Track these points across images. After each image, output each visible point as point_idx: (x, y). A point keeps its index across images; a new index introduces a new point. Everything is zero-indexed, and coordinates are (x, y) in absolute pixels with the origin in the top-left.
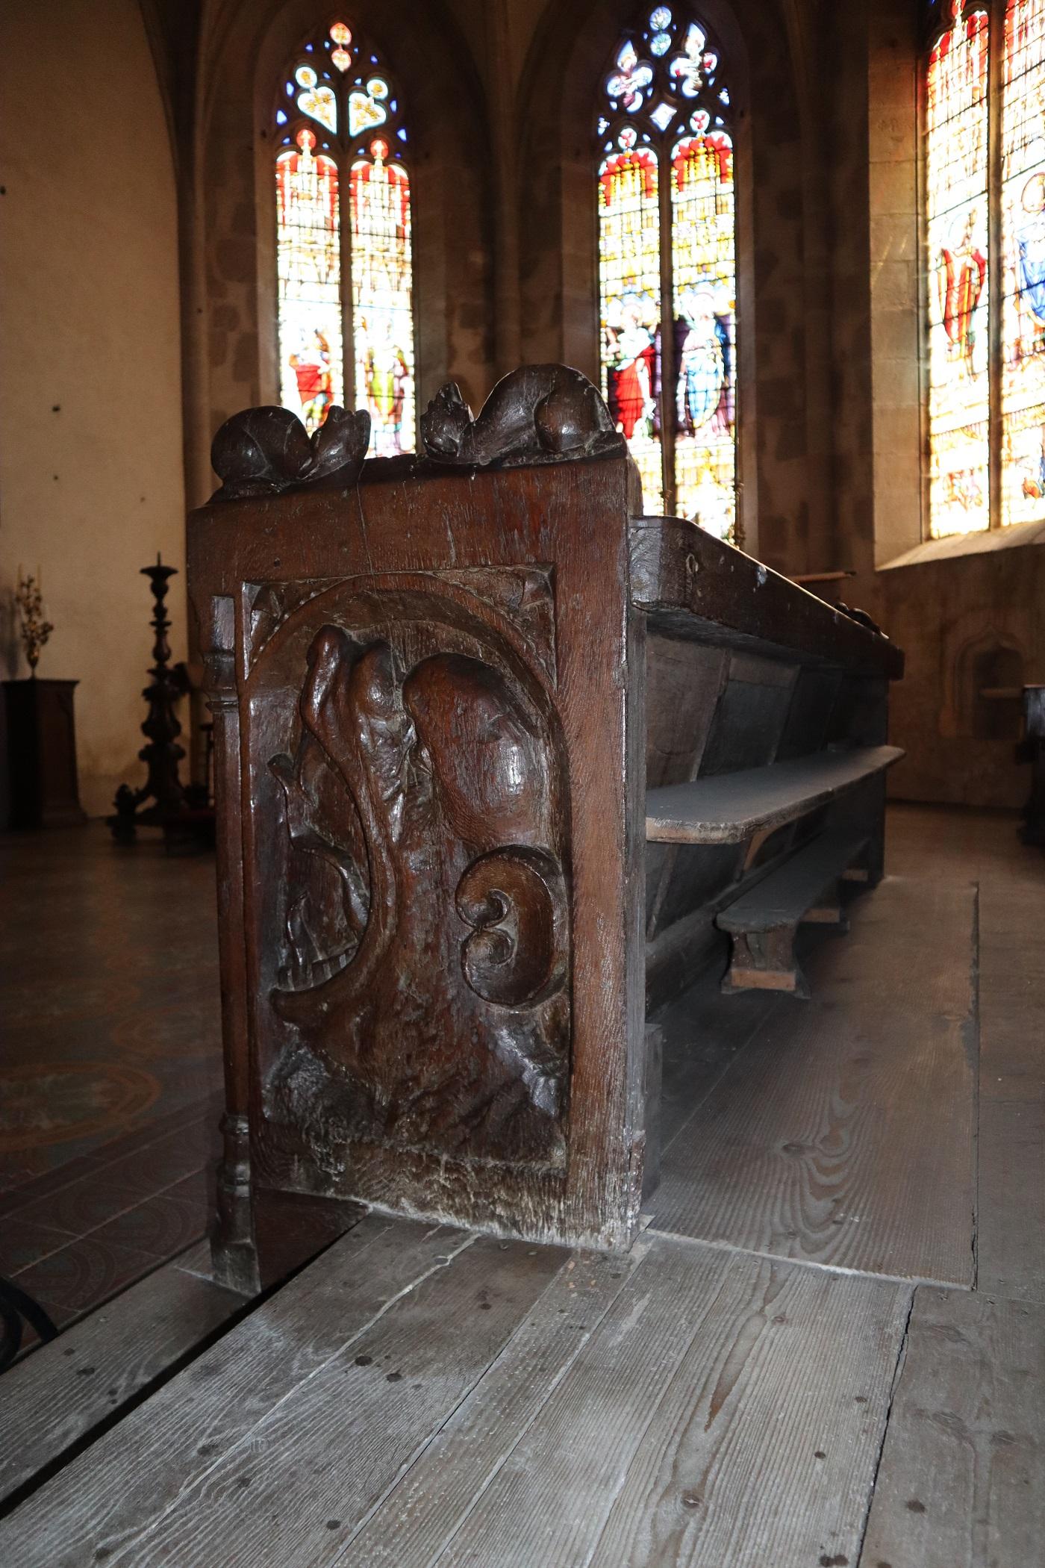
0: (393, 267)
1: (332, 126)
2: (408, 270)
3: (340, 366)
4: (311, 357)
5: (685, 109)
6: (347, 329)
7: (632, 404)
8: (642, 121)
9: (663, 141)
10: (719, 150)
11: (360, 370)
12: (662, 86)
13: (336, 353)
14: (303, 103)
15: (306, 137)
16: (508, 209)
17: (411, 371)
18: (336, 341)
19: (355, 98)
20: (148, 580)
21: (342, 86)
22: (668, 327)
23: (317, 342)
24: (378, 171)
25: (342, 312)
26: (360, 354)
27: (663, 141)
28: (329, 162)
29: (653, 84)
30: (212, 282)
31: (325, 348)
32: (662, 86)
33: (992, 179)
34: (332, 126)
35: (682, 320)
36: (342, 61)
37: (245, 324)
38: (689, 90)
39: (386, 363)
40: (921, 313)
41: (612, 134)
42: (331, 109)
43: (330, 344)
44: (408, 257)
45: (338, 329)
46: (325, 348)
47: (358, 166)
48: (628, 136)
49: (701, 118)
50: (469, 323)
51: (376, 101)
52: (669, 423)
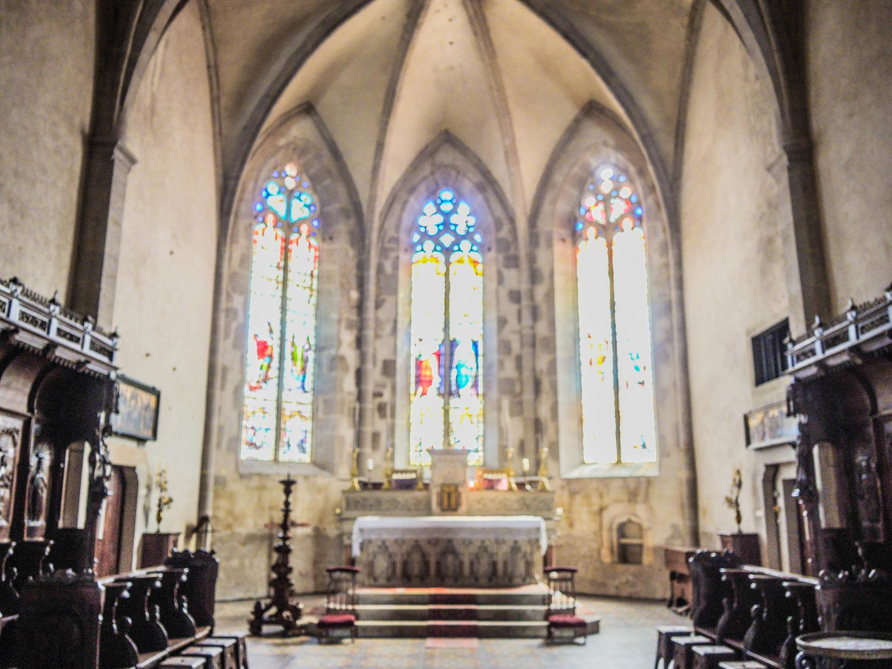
0: (308, 291)
1: (282, 213)
2: (315, 294)
3: (279, 342)
4: (264, 337)
5: (459, 239)
6: (283, 322)
7: (428, 379)
8: (436, 239)
9: (448, 251)
10: (475, 263)
11: (288, 345)
12: (446, 226)
13: (277, 334)
14: (270, 202)
15: (270, 218)
16: (372, 273)
17: (313, 348)
18: (277, 328)
19: (295, 202)
20: (282, 487)
21: (290, 194)
22: (448, 343)
23: (268, 328)
24: (303, 240)
25: (282, 313)
26: (288, 337)
27: (448, 251)
28: (281, 233)
29: (443, 224)
30: (228, 295)
31: (271, 331)
32: (446, 226)
33: (210, 45)
34: (282, 213)
35: (454, 340)
36: (290, 183)
37: (241, 318)
38: (461, 231)
39: (301, 344)
40: (577, 358)
41: (421, 242)
42: (284, 206)
43: (273, 330)
44: (315, 287)
45: (279, 322)
46: (271, 331)
47: (294, 237)
48: (429, 245)
49: (465, 244)
50: (350, 326)
51: (305, 205)
52: (447, 390)
